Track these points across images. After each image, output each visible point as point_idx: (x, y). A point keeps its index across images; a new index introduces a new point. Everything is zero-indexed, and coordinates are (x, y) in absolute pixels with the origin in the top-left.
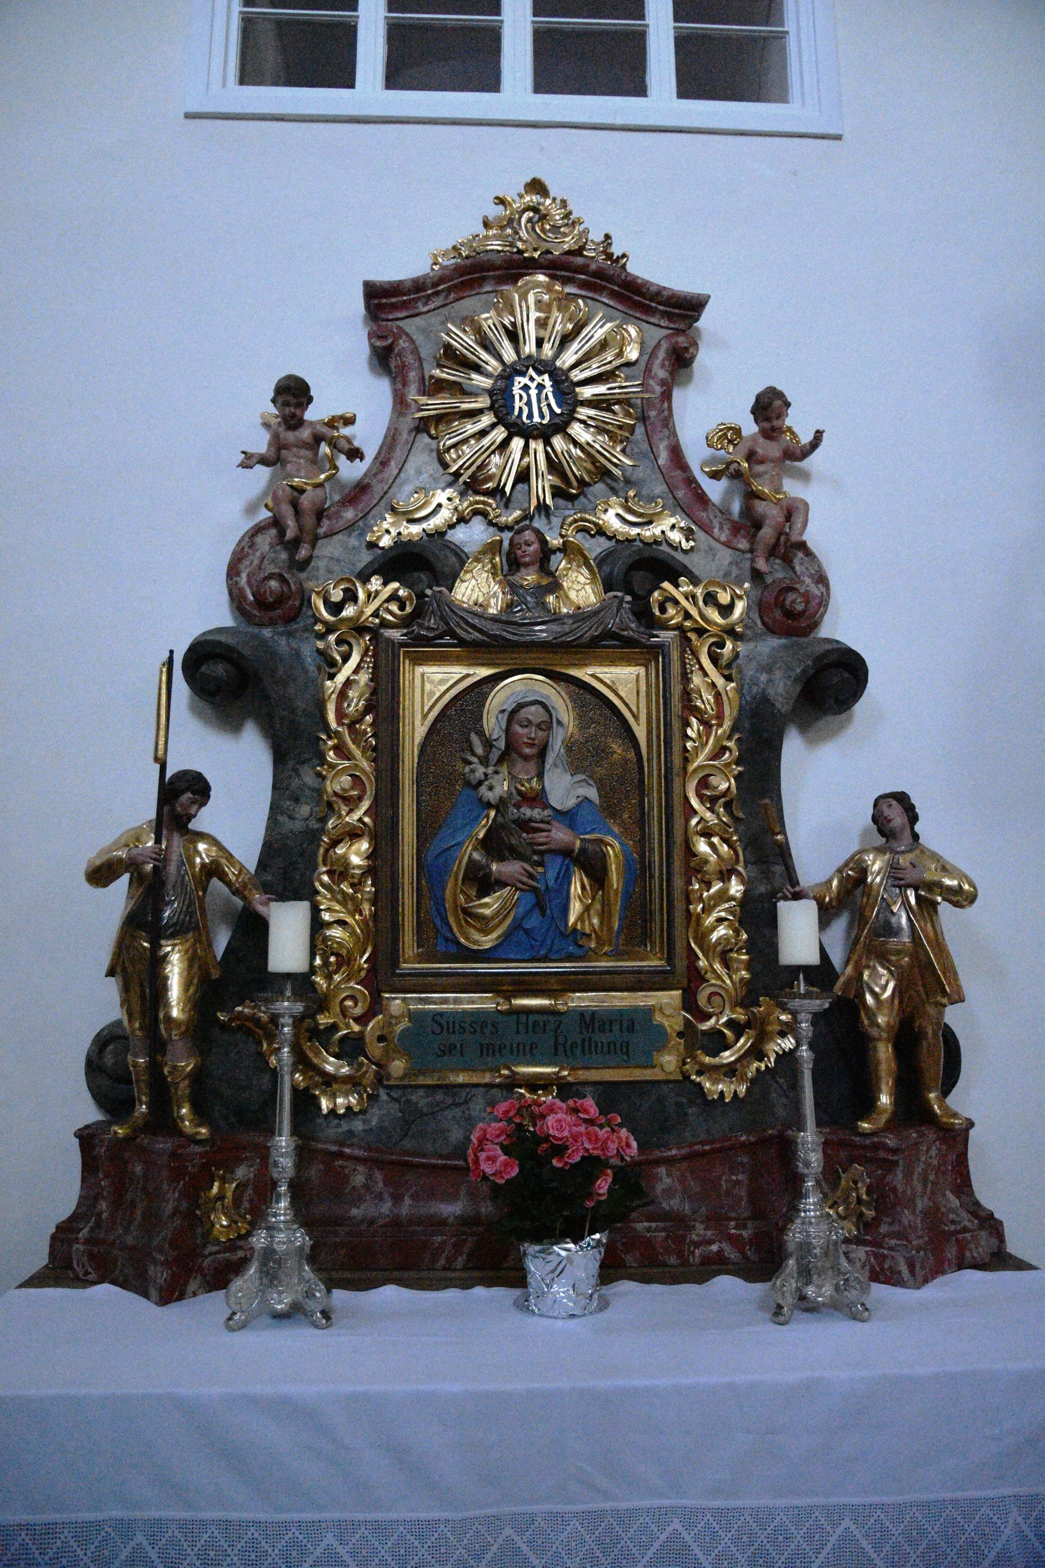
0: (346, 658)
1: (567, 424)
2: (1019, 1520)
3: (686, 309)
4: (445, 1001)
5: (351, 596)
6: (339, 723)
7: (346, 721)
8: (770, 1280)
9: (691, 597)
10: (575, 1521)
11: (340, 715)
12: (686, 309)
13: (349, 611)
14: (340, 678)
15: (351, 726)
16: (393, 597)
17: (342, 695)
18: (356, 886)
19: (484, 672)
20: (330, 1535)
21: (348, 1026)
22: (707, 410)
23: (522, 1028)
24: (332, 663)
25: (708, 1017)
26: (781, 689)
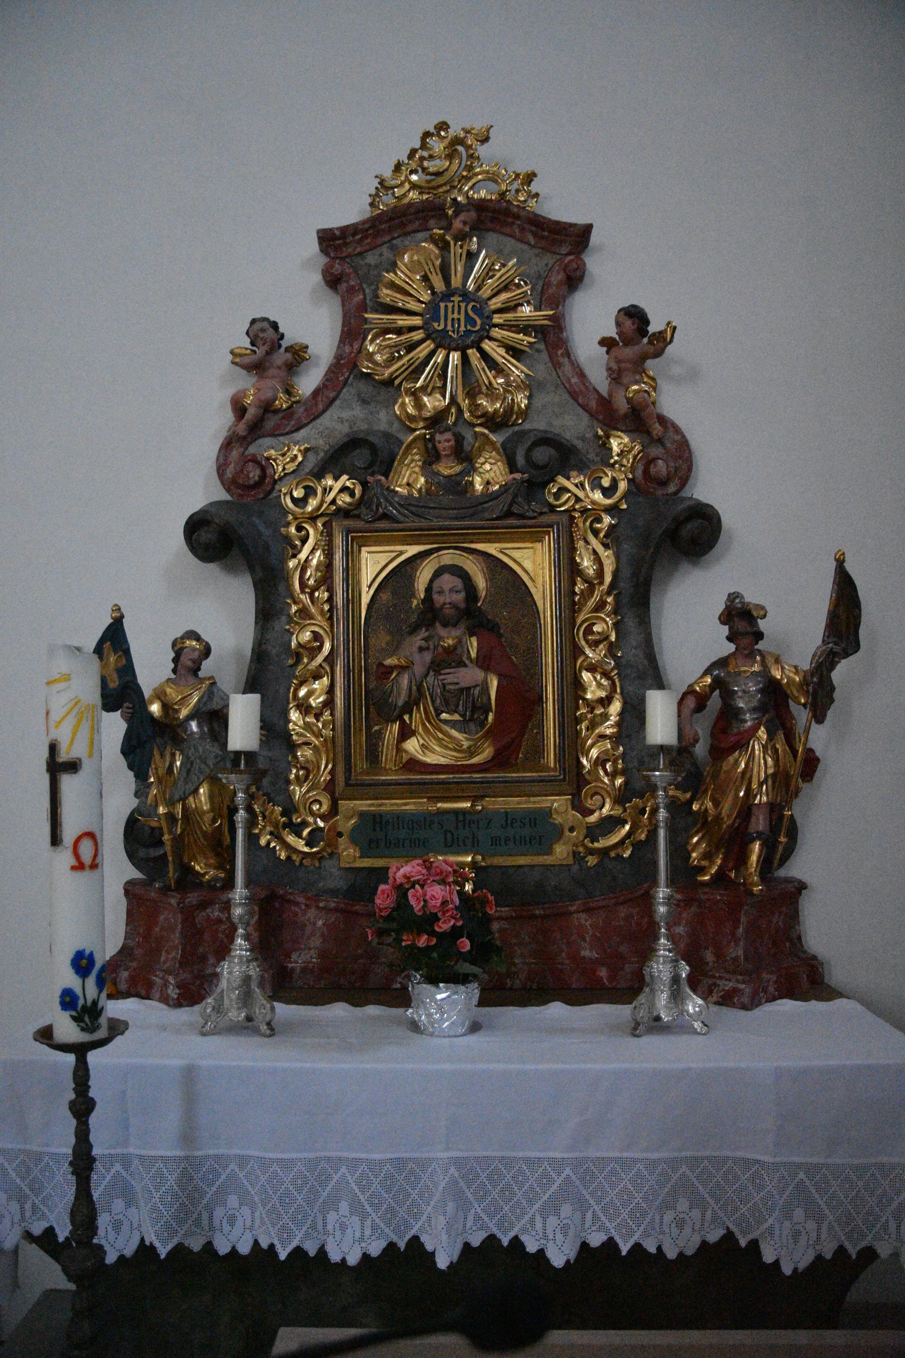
0: (304, 541)
1: (481, 340)
2: (456, 1174)
3: (579, 237)
4: (406, 804)
5: (310, 492)
6: (303, 591)
7: (307, 590)
8: (630, 1003)
9: (581, 486)
10: (388, 1165)
11: (303, 585)
12: (579, 237)
13: (312, 504)
14: (303, 556)
15: (311, 595)
16: (344, 489)
17: (304, 567)
18: (317, 716)
19: (412, 550)
20: (684, 1167)
21: (316, 822)
22: (590, 322)
23: (460, 825)
24: (294, 547)
25: (592, 812)
26: (283, 373)
